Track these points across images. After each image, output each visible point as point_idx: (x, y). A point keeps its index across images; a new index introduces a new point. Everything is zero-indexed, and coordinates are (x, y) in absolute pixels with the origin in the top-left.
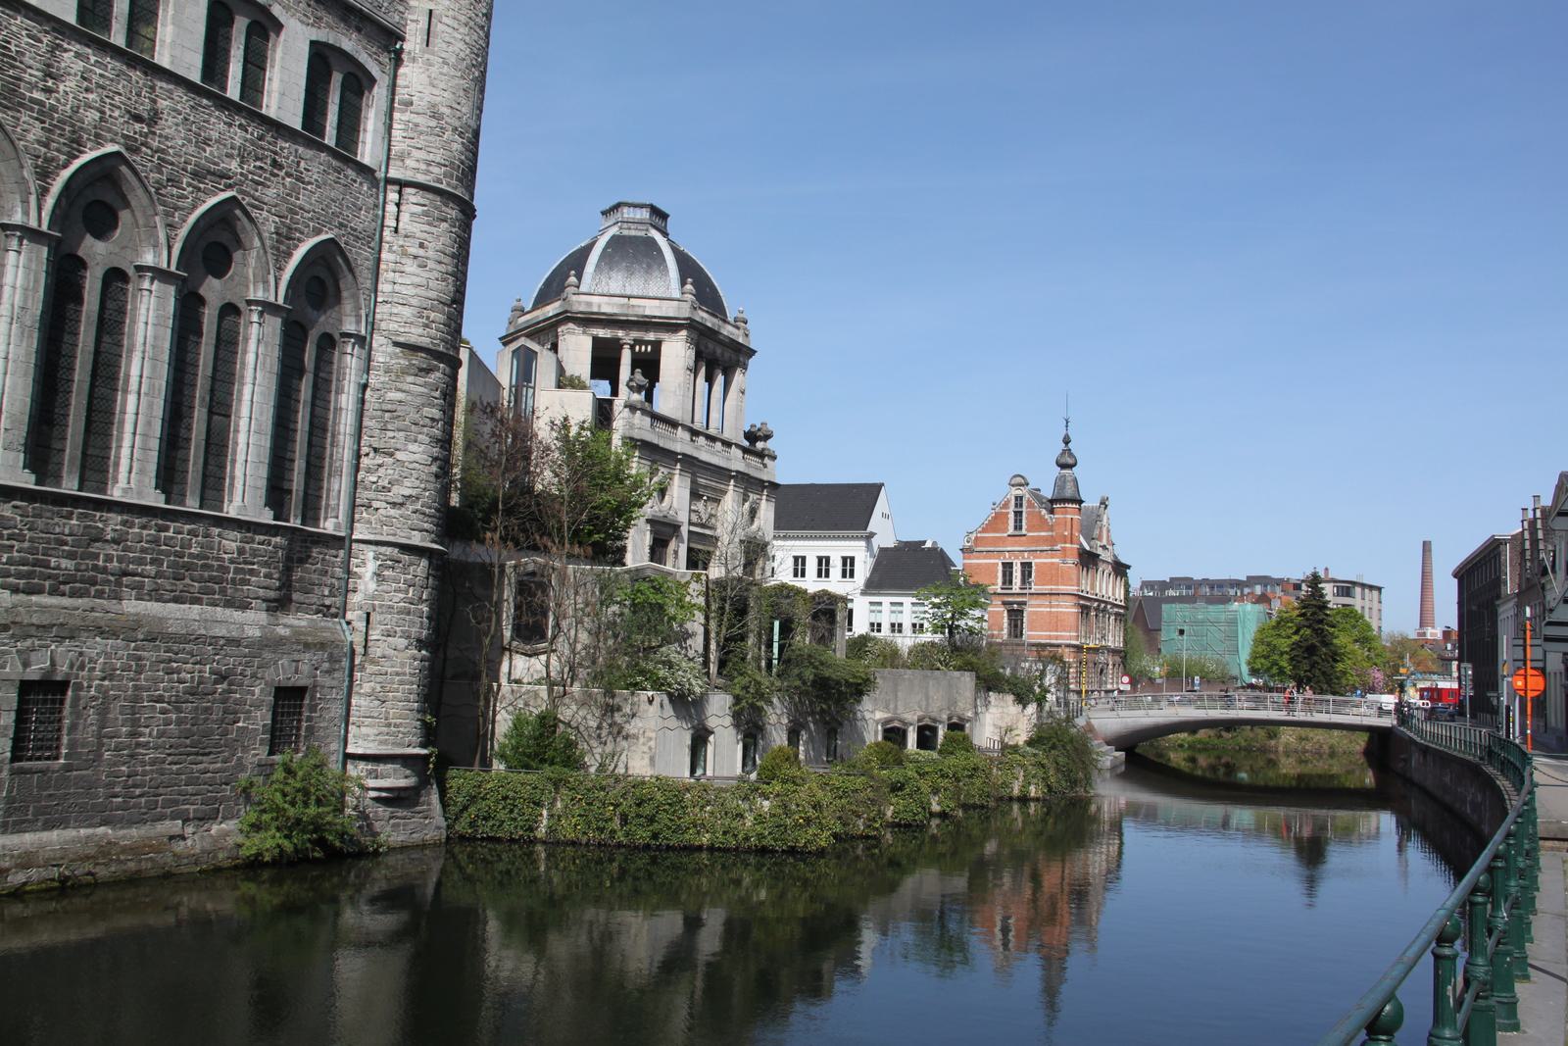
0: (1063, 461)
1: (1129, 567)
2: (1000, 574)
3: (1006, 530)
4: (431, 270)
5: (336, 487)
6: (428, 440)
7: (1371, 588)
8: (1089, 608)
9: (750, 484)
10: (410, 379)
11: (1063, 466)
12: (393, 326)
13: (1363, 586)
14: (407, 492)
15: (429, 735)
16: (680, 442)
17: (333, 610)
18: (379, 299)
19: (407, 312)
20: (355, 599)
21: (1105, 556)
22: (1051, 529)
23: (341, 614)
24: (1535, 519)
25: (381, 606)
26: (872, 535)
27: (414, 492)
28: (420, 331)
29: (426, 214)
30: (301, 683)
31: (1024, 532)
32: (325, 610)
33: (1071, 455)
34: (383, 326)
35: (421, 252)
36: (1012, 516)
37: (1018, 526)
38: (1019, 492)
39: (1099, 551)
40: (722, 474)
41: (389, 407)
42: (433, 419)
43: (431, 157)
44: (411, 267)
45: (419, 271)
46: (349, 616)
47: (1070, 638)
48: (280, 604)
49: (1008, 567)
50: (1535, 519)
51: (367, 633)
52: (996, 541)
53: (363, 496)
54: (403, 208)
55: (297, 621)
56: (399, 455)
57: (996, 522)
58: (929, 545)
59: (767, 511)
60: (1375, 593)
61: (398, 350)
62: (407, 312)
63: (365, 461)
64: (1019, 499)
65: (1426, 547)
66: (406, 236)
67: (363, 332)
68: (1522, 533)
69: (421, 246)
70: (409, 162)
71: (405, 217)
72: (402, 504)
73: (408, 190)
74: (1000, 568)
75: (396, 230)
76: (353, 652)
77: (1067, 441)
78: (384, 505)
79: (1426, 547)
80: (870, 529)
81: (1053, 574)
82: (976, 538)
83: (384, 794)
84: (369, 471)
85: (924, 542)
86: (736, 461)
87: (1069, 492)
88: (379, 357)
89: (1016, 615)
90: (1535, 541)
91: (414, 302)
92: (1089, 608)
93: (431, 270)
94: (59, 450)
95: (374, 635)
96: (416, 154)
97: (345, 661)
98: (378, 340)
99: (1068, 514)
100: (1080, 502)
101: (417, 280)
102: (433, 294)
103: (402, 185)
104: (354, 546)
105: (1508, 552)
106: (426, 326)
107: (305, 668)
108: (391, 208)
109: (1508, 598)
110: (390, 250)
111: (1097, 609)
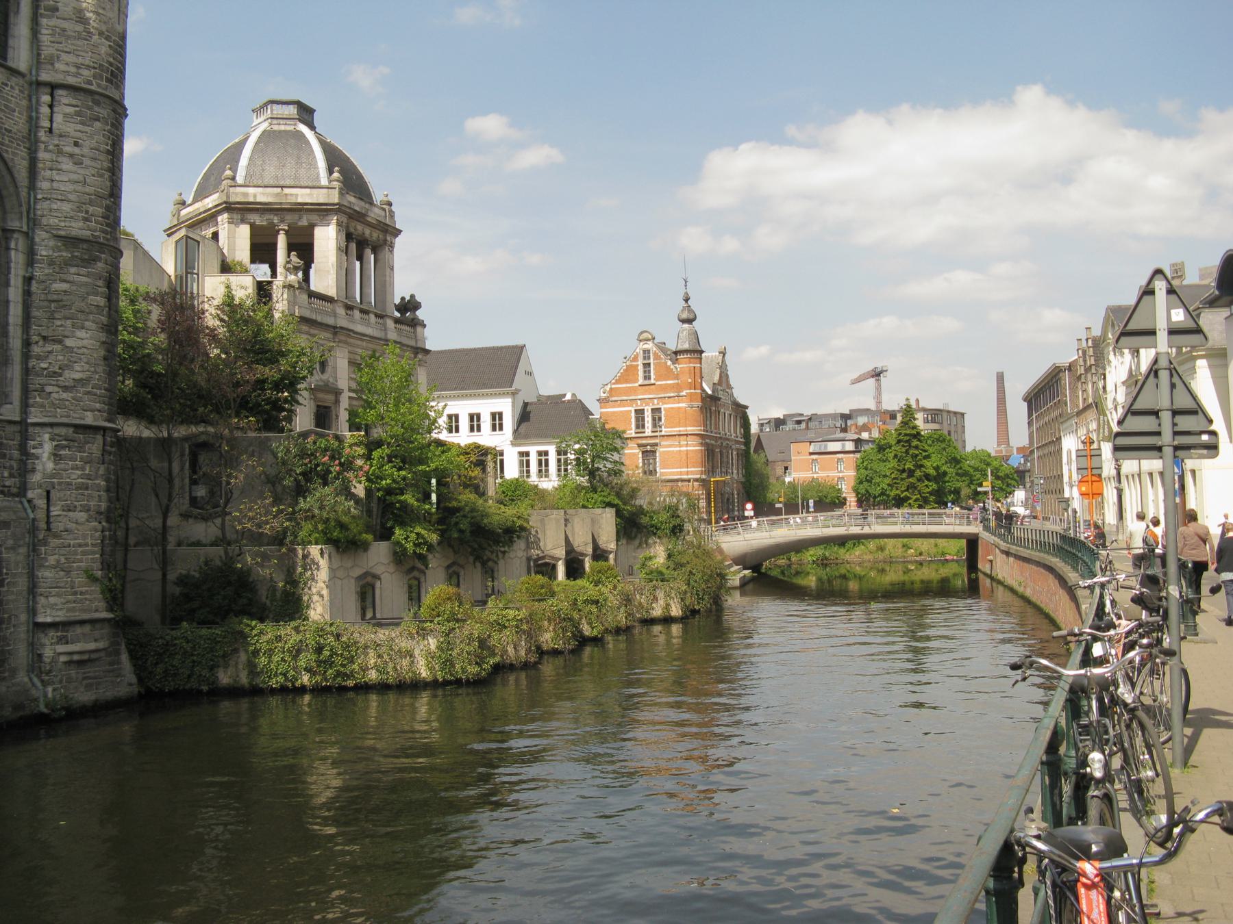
0: (685, 316)
2: (633, 420)
3: (637, 380)
11: (683, 321)
19: (66, 207)
20: (36, 478)
22: (677, 377)
25: (60, 484)
28: (80, 224)
29: (78, 114)
35: (77, 150)
36: (641, 368)
37: (647, 377)
38: (646, 346)
41: (55, 297)
43: (80, 60)
45: (74, 168)
46: (30, 494)
49: (639, 413)
51: (48, 511)
54: (55, 109)
57: (628, 374)
58: (568, 397)
63: (36, 349)
65: (1000, 378)
66: (61, 136)
69: (76, 144)
70: (59, 66)
71: (58, 118)
73: (59, 92)
74: (633, 414)
75: (51, 130)
78: (56, 389)
79: (1000, 378)
83: (76, 657)
87: (686, 346)
88: (43, 252)
91: (72, 197)
93: (87, 167)
95: (55, 511)
96: (64, 56)
98: (40, 235)
101: (74, 177)
103: (53, 87)
106: (86, 219)
108: (45, 110)
110: (46, 150)
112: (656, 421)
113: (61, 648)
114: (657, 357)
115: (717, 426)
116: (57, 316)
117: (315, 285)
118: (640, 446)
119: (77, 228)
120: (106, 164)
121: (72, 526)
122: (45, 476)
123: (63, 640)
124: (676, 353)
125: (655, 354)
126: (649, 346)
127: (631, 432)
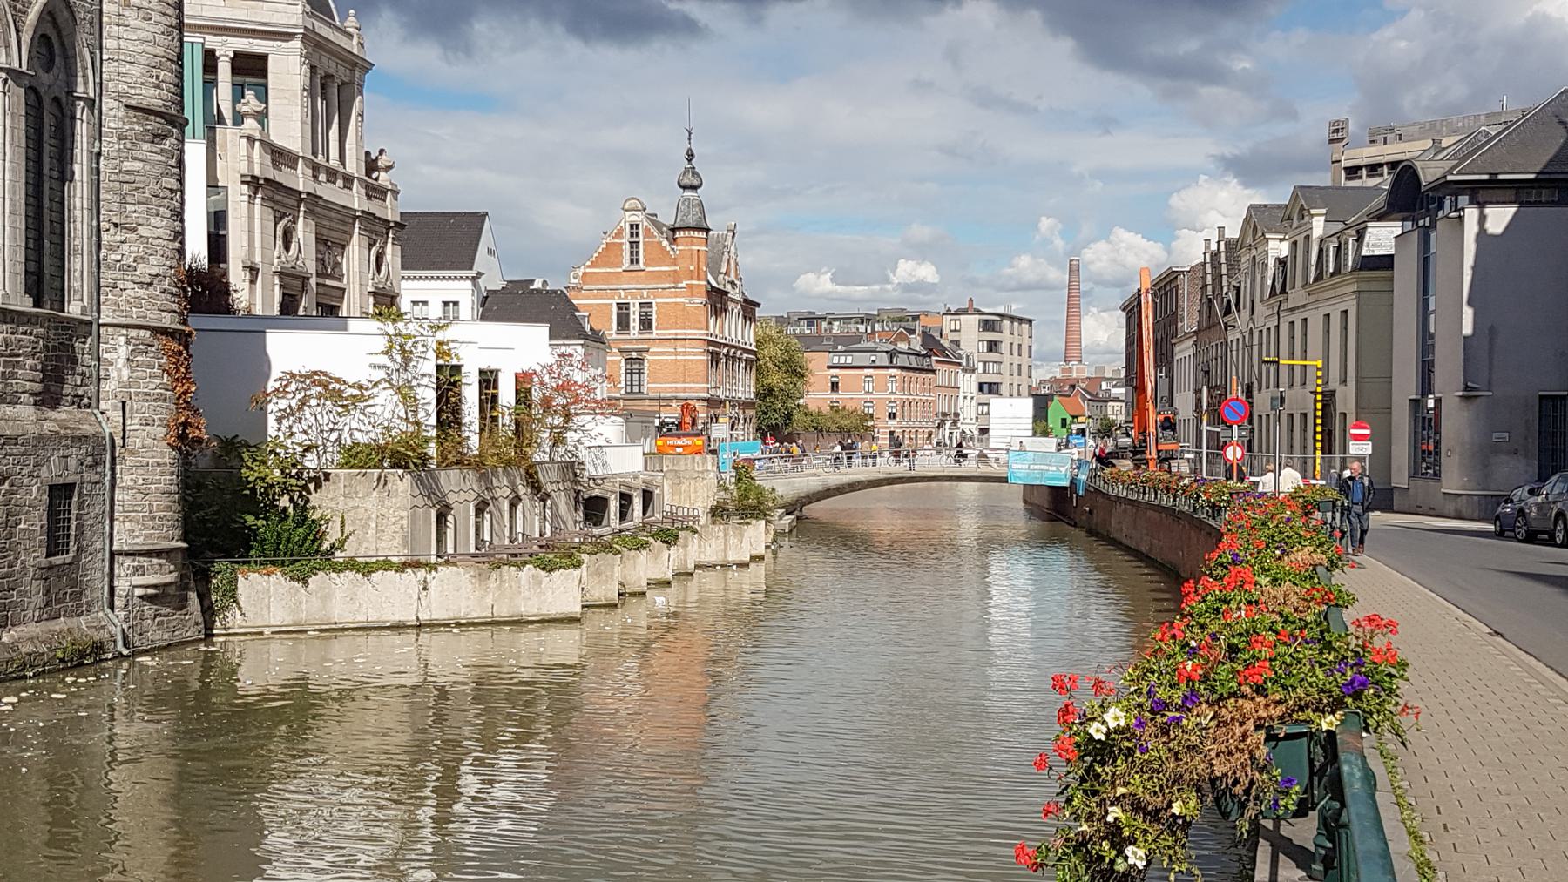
0: (686, 181)
1: (758, 305)
2: (614, 317)
3: (620, 264)
4: (156, 23)
5: (78, 267)
6: (169, 213)
7: (1021, 320)
8: (720, 355)
9: (376, 227)
10: (146, 146)
11: (684, 188)
12: (123, 88)
13: (1012, 318)
14: (155, 271)
15: (189, 529)
16: (299, 179)
17: (86, 401)
18: (105, 57)
19: (136, 71)
20: (109, 386)
21: (734, 294)
22: (674, 262)
23: (94, 404)
24: (1219, 252)
25: (137, 394)
26: (480, 274)
27: (161, 271)
30: (70, 480)
31: (642, 266)
32: (77, 401)
33: (695, 174)
34: (111, 86)
36: (626, 247)
38: (634, 219)
39: (728, 288)
40: (347, 217)
41: (127, 178)
42: (171, 191)
44: (134, 19)
45: (144, 24)
46: (103, 406)
47: (701, 390)
48: (48, 398)
49: (623, 310)
50: (1219, 252)
52: (607, 278)
53: (107, 276)
55: (64, 413)
56: (141, 230)
58: (537, 285)
59: (392, 254)
60: (1025, 326)
61: (131, 113)
62: (136, 71)
63: (105, 237)
64: (634, 227)
67: (92, 95)
68: (1204, 264)
72: (150, 284)
74: (615, 309)
76: (113, 441)
77: (690, 156)
78: (131, 285)
80: (477, 267)
81: (677, 315)
82: (585, 274)
83: (150, 591)
84: (110, 248)
85: (532, 282)
86: (356, 200)
87: (690, 222)
88: (110, 124)
89: (634, 363)
90: (1218, 277)
91: (142, 59)
92: (720, 355)
93: (156, 23)
94: (1495, 449)
95: (133, 424)
97: (103, 453)
98: (108, 104)
99: (692, 244)
100: (707, 230)
101: (144, 35)
102: (159, 51)
104: (103, 330)
105: (1185, 288)
106: (157, 87)
107: (72, 462)
109: (1187, 336)
111: (727, 355)
112: (646, 323)
113: (137, 580)
114: (648, 233)
115: (722, 331)
116: (129, 199)
117: (276, 138)
118: (621, 351)
119: (150, 97)
120: (175, 22)
121: (150, 442)
122: (121, 384)
123: (139, 571)
124: (674, 230)
125: (647, 229)
126: (637, 218)
127: (611, 332)
